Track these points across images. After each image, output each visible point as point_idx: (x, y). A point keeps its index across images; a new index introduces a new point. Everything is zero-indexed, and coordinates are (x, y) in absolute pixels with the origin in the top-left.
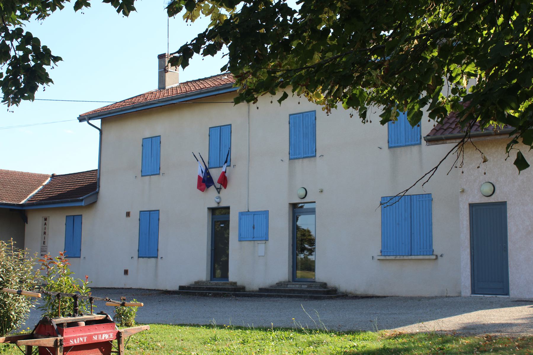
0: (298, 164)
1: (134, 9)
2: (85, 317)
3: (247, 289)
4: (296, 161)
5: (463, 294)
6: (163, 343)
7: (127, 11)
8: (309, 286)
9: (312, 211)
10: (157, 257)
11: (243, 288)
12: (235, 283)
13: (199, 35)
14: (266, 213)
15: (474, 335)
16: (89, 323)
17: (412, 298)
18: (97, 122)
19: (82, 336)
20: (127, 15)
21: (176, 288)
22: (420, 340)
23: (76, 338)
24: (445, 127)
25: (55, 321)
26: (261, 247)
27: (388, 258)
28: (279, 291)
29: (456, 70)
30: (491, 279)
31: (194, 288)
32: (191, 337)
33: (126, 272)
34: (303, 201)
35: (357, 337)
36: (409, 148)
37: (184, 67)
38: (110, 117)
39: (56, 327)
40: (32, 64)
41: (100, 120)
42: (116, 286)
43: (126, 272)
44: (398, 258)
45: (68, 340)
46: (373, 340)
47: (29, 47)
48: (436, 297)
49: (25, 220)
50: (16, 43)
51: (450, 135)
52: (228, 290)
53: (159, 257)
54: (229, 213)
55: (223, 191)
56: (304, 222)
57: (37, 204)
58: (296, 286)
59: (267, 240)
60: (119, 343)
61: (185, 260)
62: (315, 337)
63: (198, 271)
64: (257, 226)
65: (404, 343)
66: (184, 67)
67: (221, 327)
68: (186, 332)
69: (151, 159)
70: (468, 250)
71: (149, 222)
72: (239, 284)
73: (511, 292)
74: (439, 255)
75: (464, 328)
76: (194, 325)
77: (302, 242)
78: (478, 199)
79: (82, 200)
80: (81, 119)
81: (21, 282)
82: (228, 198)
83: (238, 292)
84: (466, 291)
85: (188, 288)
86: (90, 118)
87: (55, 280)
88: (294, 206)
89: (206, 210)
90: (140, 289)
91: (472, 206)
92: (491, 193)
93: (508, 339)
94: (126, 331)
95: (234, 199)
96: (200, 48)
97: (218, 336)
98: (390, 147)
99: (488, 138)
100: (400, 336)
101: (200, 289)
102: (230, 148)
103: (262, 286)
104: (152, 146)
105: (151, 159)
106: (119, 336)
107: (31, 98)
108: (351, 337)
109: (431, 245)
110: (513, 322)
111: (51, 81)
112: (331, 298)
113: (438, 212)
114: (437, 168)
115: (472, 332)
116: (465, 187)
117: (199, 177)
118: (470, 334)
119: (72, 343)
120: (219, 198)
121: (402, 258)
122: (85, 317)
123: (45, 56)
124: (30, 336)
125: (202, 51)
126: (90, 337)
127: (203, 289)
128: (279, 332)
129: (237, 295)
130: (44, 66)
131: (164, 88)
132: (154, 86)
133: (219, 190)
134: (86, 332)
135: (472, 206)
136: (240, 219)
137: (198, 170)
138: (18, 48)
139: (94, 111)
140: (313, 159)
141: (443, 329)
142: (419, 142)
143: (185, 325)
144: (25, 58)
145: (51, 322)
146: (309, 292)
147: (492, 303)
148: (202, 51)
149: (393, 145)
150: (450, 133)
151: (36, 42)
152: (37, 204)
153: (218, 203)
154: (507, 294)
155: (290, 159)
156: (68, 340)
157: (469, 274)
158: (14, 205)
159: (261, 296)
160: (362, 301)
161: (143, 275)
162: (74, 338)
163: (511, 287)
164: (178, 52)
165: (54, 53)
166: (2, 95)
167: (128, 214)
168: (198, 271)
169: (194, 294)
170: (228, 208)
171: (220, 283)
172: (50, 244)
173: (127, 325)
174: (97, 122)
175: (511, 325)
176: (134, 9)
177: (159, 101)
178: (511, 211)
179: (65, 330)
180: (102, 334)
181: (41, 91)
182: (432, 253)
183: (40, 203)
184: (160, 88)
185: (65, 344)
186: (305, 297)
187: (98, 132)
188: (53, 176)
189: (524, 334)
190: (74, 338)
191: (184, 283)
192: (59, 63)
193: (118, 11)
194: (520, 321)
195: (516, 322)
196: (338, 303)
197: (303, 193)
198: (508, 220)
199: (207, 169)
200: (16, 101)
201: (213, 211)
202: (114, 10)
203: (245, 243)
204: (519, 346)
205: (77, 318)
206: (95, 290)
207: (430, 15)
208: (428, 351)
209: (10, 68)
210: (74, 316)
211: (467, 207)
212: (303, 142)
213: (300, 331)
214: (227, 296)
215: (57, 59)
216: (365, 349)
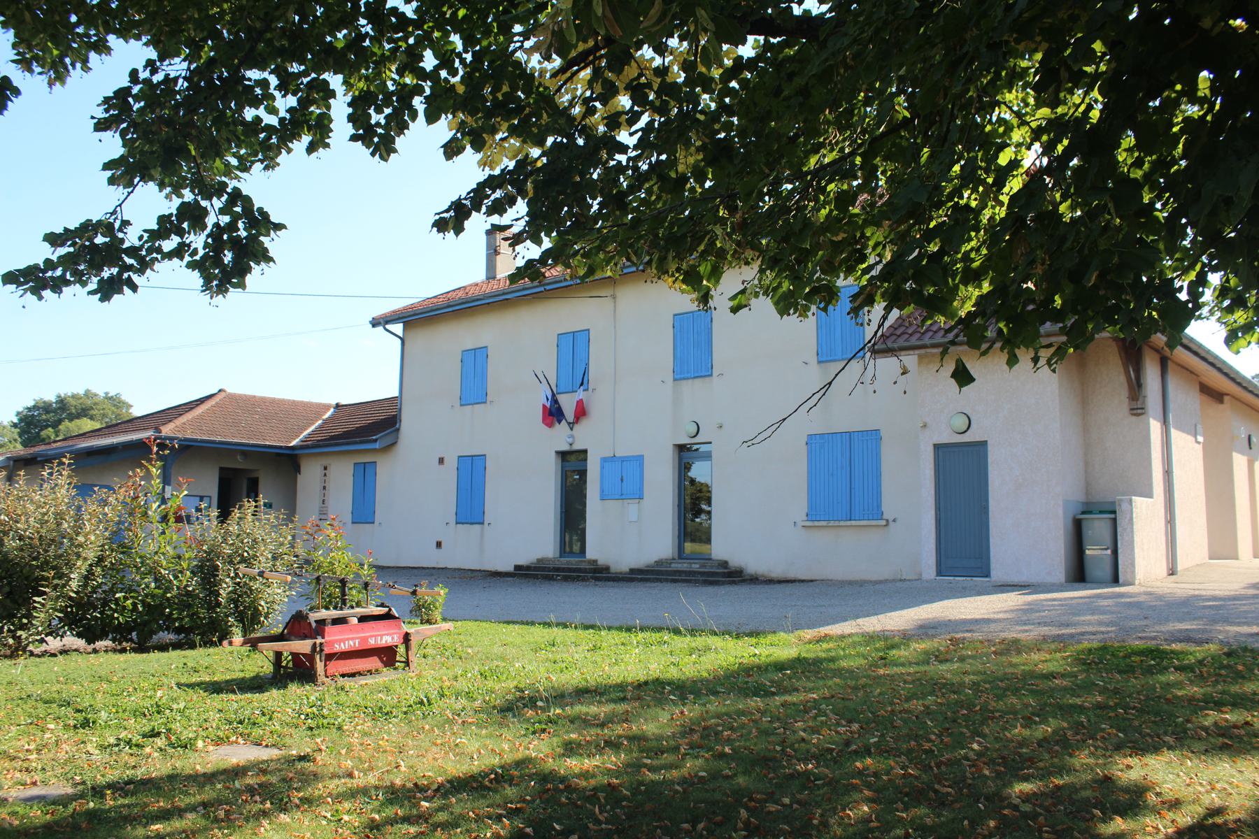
0: (687, 386)
1: (395, 151)
4: (684, 382)
5: (925, 576)
6: (476, 649)
7: (385, 154)
8: (703, 566)
9: (708, 456)
10: (482, 523)
11: (607, 569)
12: (595, 561)
13: (478, 184)
14: (640, 459)
15: (934, 636)
16: (363, 619)
17: (851, 583)
18: (398, 328)
20: (386, 160)
21: (511, 569)
22: (854, 645)
23: (344, 641)
24: (898, 332)
25: (314, 617)
26: (632, 508)
28: (658, 573)
29: (876, 236)
31: (536, 569)
32: (518, 640)
33: (439, 545)
35: (762, 640)
37: (457, 233)
38: (416, 319)
39: (314, 625)
40: (243, 234)
42: (425, 565)
43: (439, 545)
44: (832, 523)
45: (331, 643)
46: (790, 645)
47: (238, 209)
48: (886, 581)
49: (297, 469)
50: (218, 203)
51: (919, 343)
52: (585, 571)
54: (586, 460)
55: (576, 427)
56: (699, 471)
57: (314, 447)
58: (684, 566)
59: (641, 498)
60: (407, 649)
61: (523, 526)
62: (700, 641)
63: (541, 542)
65: (829, 650)
66: (457, 233)
68: (513, 633)
69: (474, 383)
70: (933, 512)
71: (472, 472)
73: (993, 573)
74: (891, 519)
75: (921, 627)
76: (527, 623)
77: (694, 503)
79: (375, 441)
80: (375, 323)
81: (275, 558)
82: (583, 437)
83: (600, 574)
84: (929, 571)
85: (528, 568)
86: (387, 322)
87: (325, 555)
88: (681, 448)
89: (671, 448)
90: (459, 570)
91: (937, 447)
93: (981, 642)
94: (417, 632)
96: (481, 204)
97: (558, 640)
98: (819, 362)
100: (825, 638)
101: (544, 569)
102: (587, 364)
103: (634, 565)
104: (475, 360)
105: (474, 383)
106: (407, 638)
107: (242, 285)
108: (754, 640)
109: (879, 506)
110: (992, 616)
111: (270, 259)
112: (734, 583)
113: (890, 457)
114: (830, 383)
115: (931, 632)
117: (544, 406)
118: (927, 635)
119: (338, 648)
120: (572, 436)
121: (837, 523)
123: (262, 223)
124: (280, 638)
125: (484, 209)
126: (364, 640)
127: (549, 570)
128: (647, 634)
129: (597, 579)
130: (262, 238)
131: (494, 278)
132: (479, 275)
133: (571, 425)
134: (358, 632)
135: (937, 447)
136: (602, 468)
137: (540, 397)
138: (222, 211)
141: (889, 628)
143: (514, 623)
144: (232, 226)
147: (964, 588)
148: (484, 209)
150: (919, 339)
151: (247, 201)
152: (314, 447)
154: (988, 575)
155: (675, 380)
156: (331, 643)
158: (281, 447)
159: (631, 580)
160: (777, 586)
161: (465, 550)
162: (339, 641)
163: (993, 565)
164: (447, 211)
165: (274, 219)
166: (201, 281)
167: (441, 461)
168: (541, 542)
169: (535, 577)
170: (585, 451)
171: (572, 561)
172: (331, 502)
173: (429, 622)
174: (398, 328)
175: (988, 621)
176: (395, 151)
177: (486, 296)
178: (994, 455)
179: (329, 629)
180: (381, 636)
181: (257, 276)
183: (317, 445)
184: (488, 278)
185: (327, 650)
186: (696, 582)
187: (399, 341)
188: (338, 406)
189: (1003, 635)
191: (522, 561)
192: (281, 233)
193: (373, 154)
194: (1001, 616)
195: (996, 616)
196: (767, 588)
199: (553, 395)
200: (222, 290)
202: (368, 152)
204: (995, 653)
205: (346, 612)
206: (380, 569)
207: (832, 150)
208: (863, 662)
209: (210, 240)
211: (931, 449)
212: (693, 358)
213: (677, 632)
214: (584, 580)
215: (279, 227)
216: (772, 659)
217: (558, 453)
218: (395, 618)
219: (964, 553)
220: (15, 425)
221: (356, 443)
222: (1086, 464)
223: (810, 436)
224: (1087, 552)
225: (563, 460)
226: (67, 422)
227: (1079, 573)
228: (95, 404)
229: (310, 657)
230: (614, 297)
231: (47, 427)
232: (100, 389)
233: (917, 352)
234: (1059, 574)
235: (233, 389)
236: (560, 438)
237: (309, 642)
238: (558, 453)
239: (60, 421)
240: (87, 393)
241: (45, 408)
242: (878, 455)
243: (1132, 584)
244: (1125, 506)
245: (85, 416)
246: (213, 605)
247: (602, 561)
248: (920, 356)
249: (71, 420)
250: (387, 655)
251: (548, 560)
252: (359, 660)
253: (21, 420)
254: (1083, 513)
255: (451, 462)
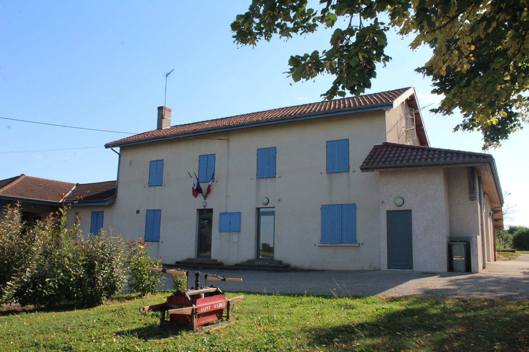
0: (263, 182)
3: (225, 264)
4: (262, 180)
10: (158, 242)
12: (216, 260)
14: (239, 214)
18: (118, 149)
19: (208, 306)
26: (235, 236)
27: (326, 245)
38: (127, 146)
39: (190, 298)
41: (119, 148)
44: (333, 245)
45: (199, 308)
53: (160, 241)
54: (212, 213)
59: (239, 232)
60: (228, 309)
63: (190, 251)
64: (232, 223)
69: (156, 176)
70: (386, 240)
72: (219, 260)
73: (414, 267)
74: (361, 243)
78: (393, 208)
79: (105, 201)
80: (107, 146)
83: (218, 267)
84: (384, 266)
89: (196, 211)
91: (388, 212)
95: (216, 203)
98: (327, 173)
99: (402, 169)
104: (156, 168)
106: (228, 303)
109: (355, 237)
113: (360, 216)
116: (384, 200)
117: (193, 188)
120: (206, 202)
121: (335, 245)
126: (212, 306)
131: (161, 129)
132: (154, 127)
135: (388, 212)
136: (220, 217)
137: (191, 183)
140: (273, 179)
145: (184, 294)
146: (272, 267)
149: (330, 171)
153: (205, 206)
155: (257, 178)
163: (414, 264)
167: (138, 212)
168: (190, 251)
174: (118, 149)
182: (356, 242)
184: (158, 129)
187: (118, 155)
188: (78, 185)
196: (293, 274)
197: (266, 201)
199: (198, 183)
201: (200, 211)
205: (200, 291)
210: (197, 289)
211: (385, 213)
218: (220, 293)
219: (401, 259)
222: (450, 221)
223: (322, 206)
224: (454, 259)
227: (451, 269)
229: (191, 317)
230: (228, 140)
233: (380, 170)
234: (444, 268)
235: (28, 174)
236: (199, 202)
243: (477, 272)
244: (474, 239)
246: (93, 284)
247: (219, 260)
248: (381, 172)
250: (218, 313)
252: (209, 317)
254: (452, 242)
255: (143, 213)
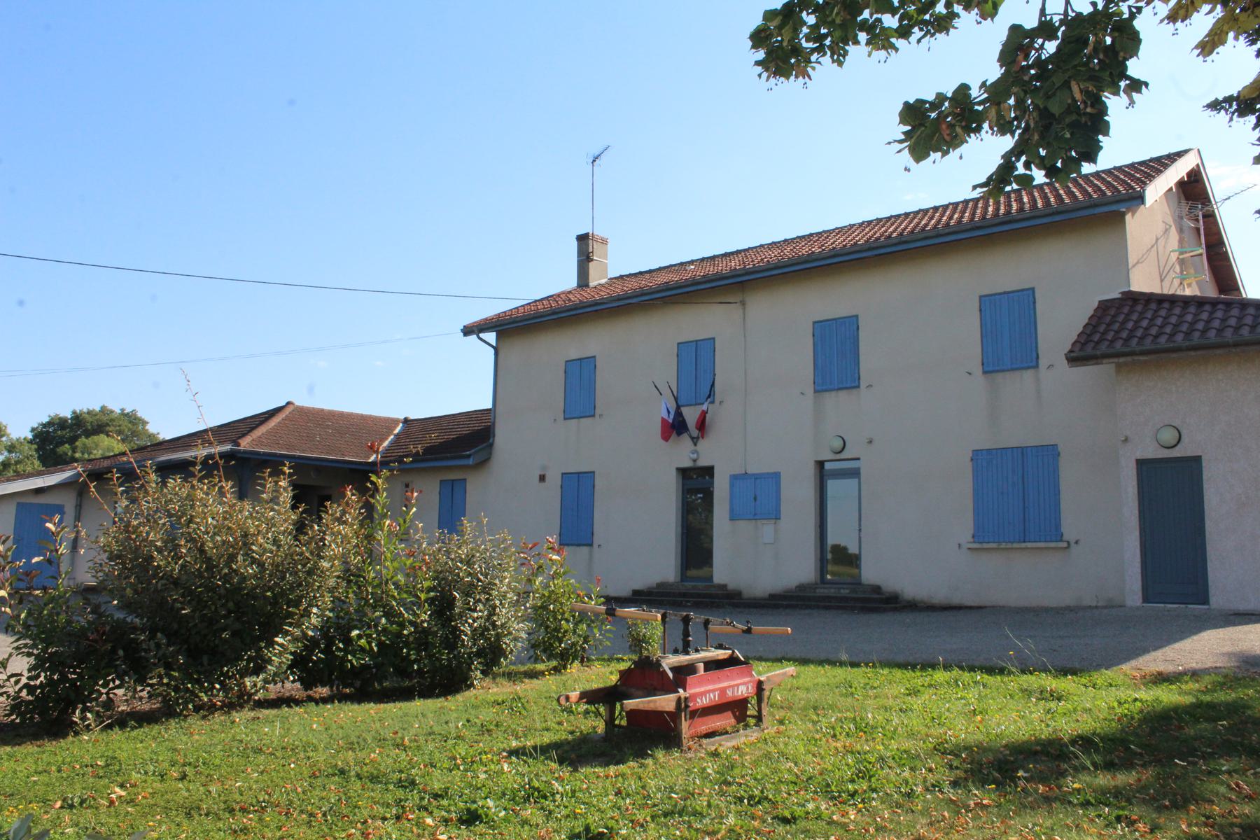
2: (703, 654)
3: (746, 594)
4: (827, 394)
10: (591, 545)
12: (725, 586)
14: (776, 476)
16: (712, 665)
18: (491, 337)
19: (713, 691)
26: (767, 529)
27: (985, 546)
30: (1178, 578)
34: (838, 457)
36: (1017, 373)
38: (511, 329)
39: (671, 675)
44: (1003, 546)
53: (595, 545)
55: (701, 443)
60: (760, 701)
63: (662, 565)
64: (760, 497)
67: (854, 665)
69: (580, 393)
70: (1137, 533)
72: (731, 586)
78: (1151, 451)
79: (469, 456)
80: (467, 331)
82: (707, 453)
83: (730, 601)
89: (674, 473)
91: (1141, 464)
92: (1174, 442)
98: (985, 372)
100: (1161, 679)
104: (581, 374)
105: (580, 393)
106: (760, 686)
113: (1070, 475)
117: (663, 420)
120: (695, 452)
121: (1009, 546)
122: (703, 654)
126: (723, 691)
131: (587, 286)
132: (571, 282)
133: (695, 440)
135: (1141, 464)
136: (732, 486)
137: (662, 409)
139: (486, 319)
140: (854, 391)
142: (1034, 364)
149: (991, 369)
153: (695, 461)
154: (1205, 601)
155: (815, 391)
157: (1139, 570)
158: (361, 463)
163: (1212, 591)
167: (542, 478)
168: (662, 565)
174: (491, 337)
178: (1211, 475)
180: (738, 685)
182: (1060, 538)
184: (579, 286)
187: (492, 351)
188: (406, 421)
190: (704, 693)
191: (639, 585)
196: (908, 617)
198: (1205, 486)
199: (678, 407)
201: (684, 473)
203: (742, 524)
211: (1133, 465)
217: (678, 469)
218: (741, 663)
220: (31, 442)
221: (447, 459)
223: (975, 452)
225: (684, 478)
226: (83, 439)
228: (112, 420)
229: (675, 716)
230: (743, 303)
231: (62, 443)
232: (117, 404)
236: (683, 453)
237: (673, 696)
238: (678, 469)
239: (75, 438)
240: (103, 409)
241: (60, 423)
242: (1056, 471)
245: (102, 432)
246: (452, 639)
248: (1119, 366)
249: (87, 437)
250: (737, 707)
251: (671, 585)
252: (715, 717)
253: (35, 436)
255: (554, 479)
